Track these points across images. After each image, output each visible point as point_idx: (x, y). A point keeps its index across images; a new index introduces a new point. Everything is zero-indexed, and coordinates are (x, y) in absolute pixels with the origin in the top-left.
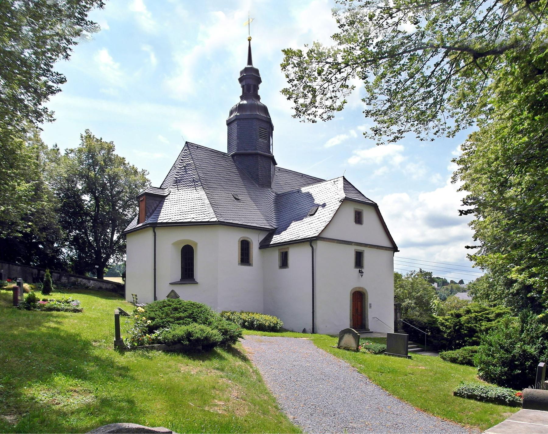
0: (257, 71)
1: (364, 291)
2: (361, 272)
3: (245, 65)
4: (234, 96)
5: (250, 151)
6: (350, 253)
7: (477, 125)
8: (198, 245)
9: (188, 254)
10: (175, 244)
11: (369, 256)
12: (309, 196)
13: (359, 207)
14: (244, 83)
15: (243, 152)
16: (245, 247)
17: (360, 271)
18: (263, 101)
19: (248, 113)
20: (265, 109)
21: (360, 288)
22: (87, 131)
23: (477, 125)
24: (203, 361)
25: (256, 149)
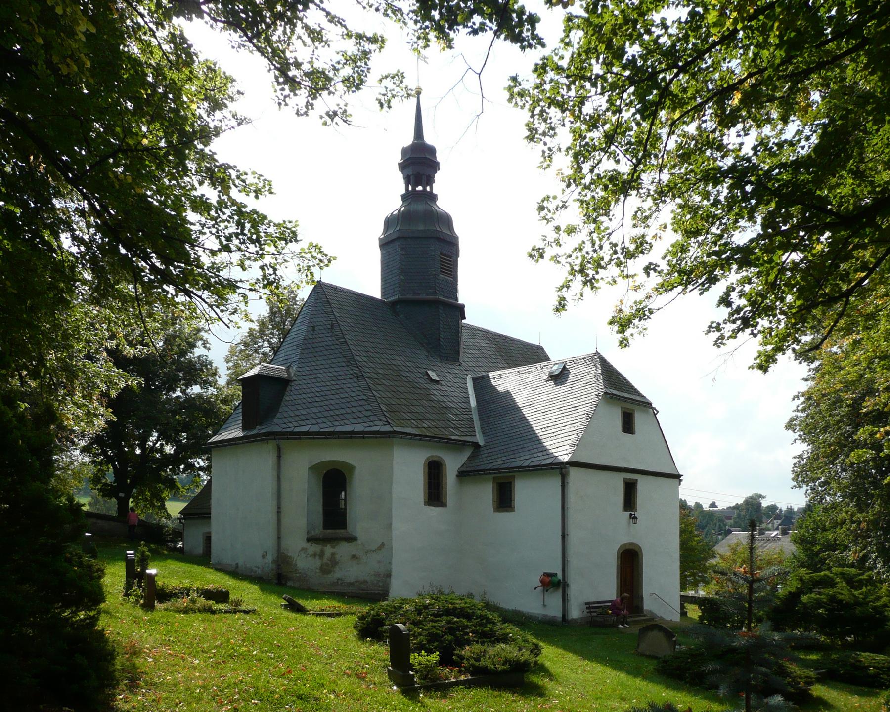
0: (432, 151)
1: (637, 549)
2: (634, 518)
3: (408, 140)
4: (391, 194)
5: (423, 297)
6: (617, 483)
7: (672, 212)
8: (357, 472)
9: (630, 489)
10: (314, 469)
11: (644, 485)
12: (229, 187)
13: (629, 406)
14: (409, 171)
15: (410, 297)
16: (434, 470)
17: (631, 515)
18: (443, 204)
19: (421, 227)
20: (447, 220)
21: (630, 544)
22: (538, 691)
23: (672, 212)
24: (318, 599)
25: (435, 293)
